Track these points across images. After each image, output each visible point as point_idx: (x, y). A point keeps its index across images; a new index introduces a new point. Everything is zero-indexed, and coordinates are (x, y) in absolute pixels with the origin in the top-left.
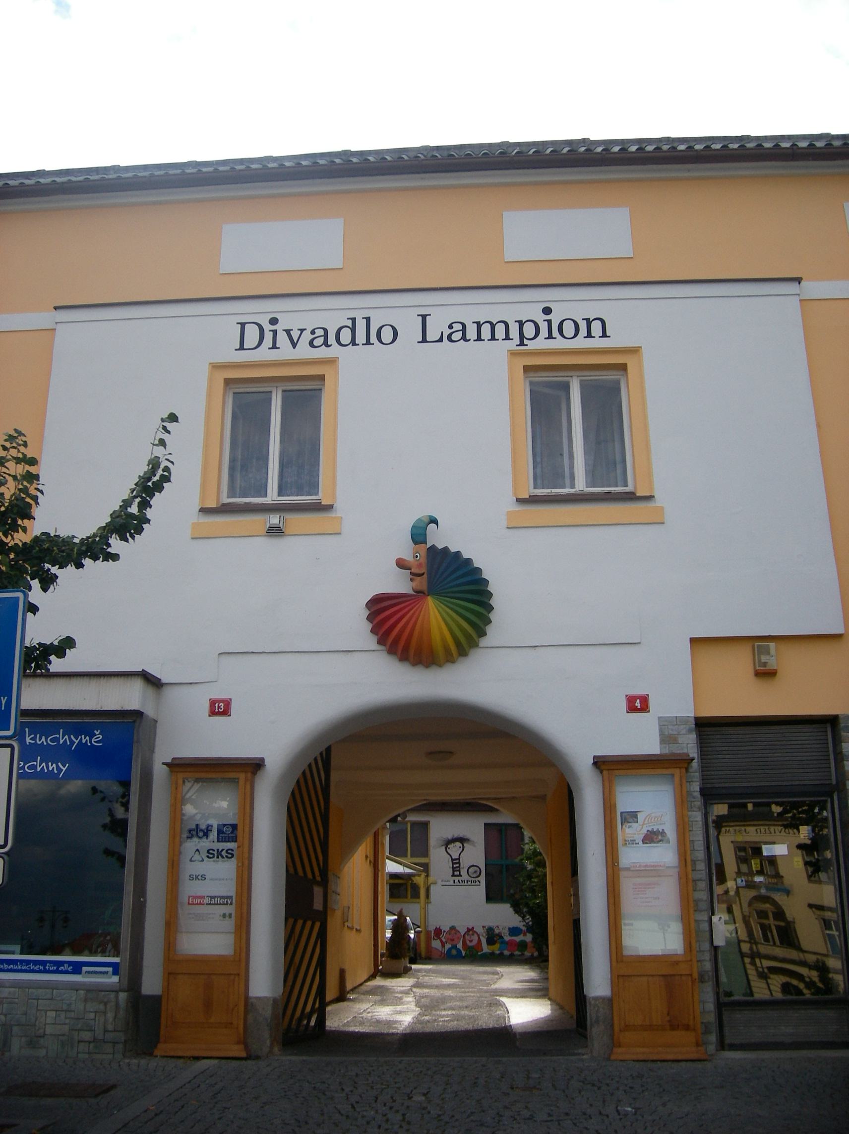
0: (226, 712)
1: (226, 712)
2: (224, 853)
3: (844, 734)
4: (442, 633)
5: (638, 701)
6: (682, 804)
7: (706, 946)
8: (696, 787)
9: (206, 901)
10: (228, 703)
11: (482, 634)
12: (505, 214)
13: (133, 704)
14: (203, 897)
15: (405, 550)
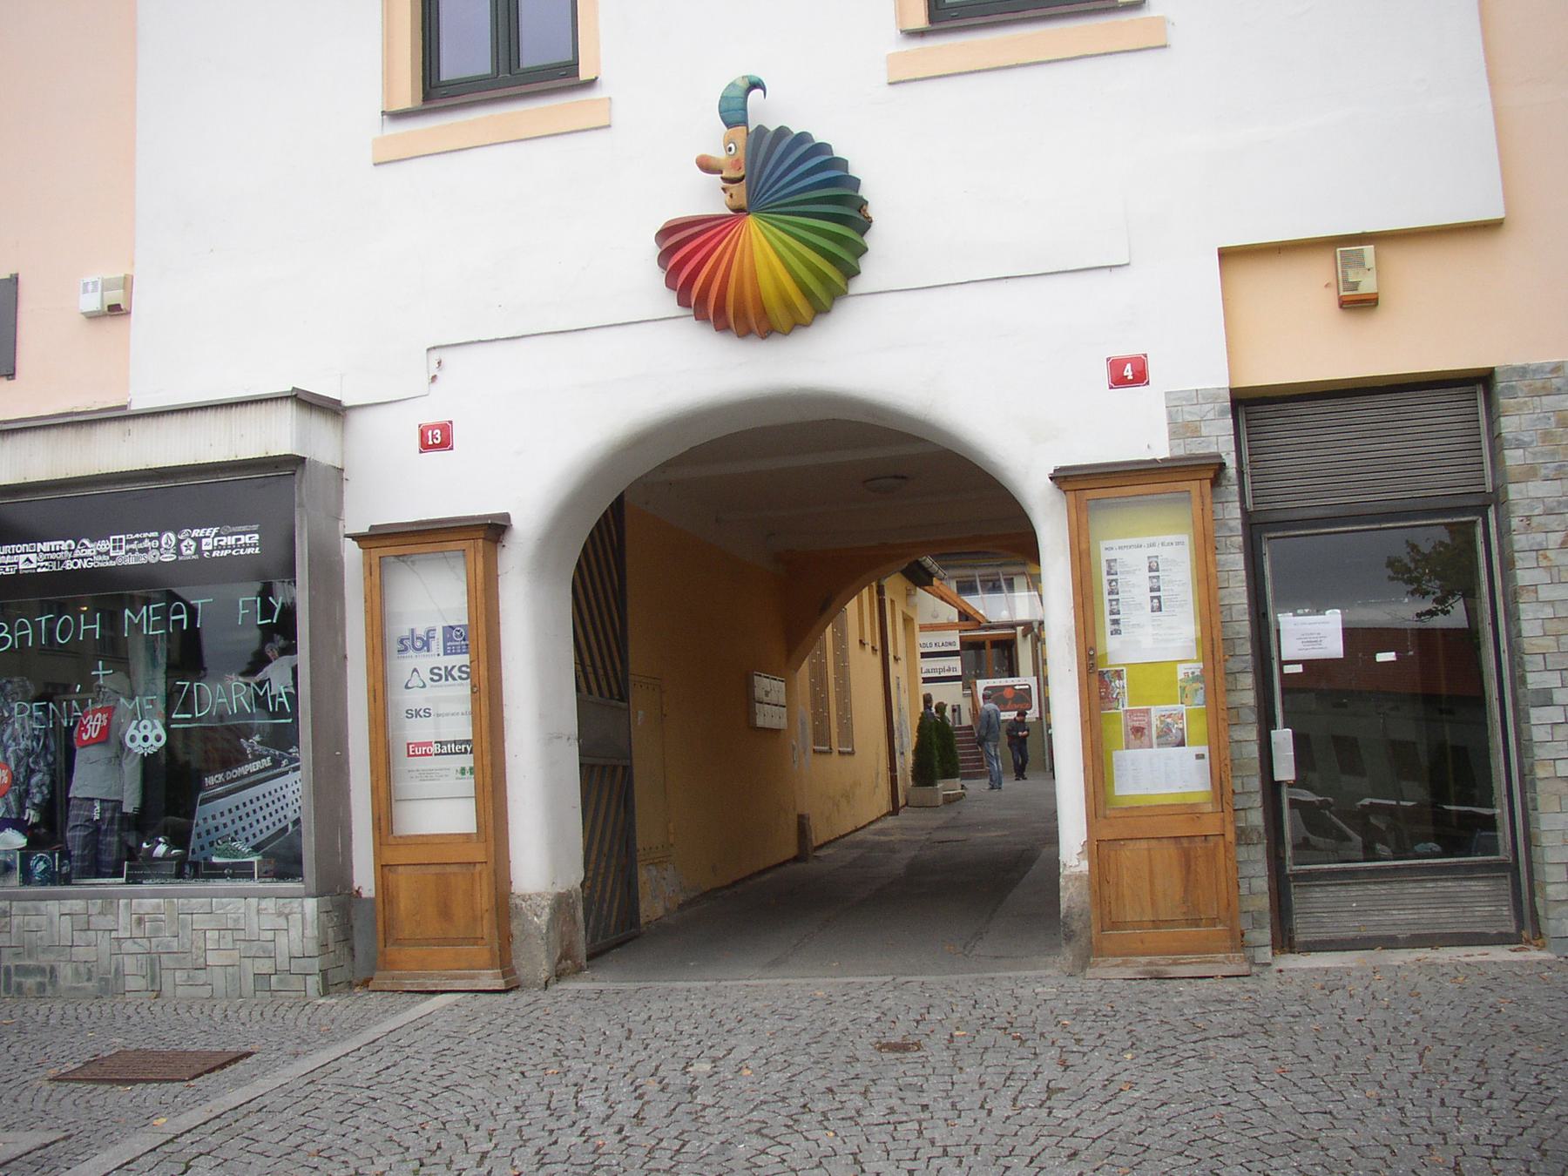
0: (446, 444)
1: (446, 444)
2: (455, 673)
3: (1503, 401)
4: (776, 280)
5: (1129, 366)
6: (1206, 548)
7: (1255, 783)
8: (1233, 513)
9: (435, 749)
10: (446, 429)
11: (851, 273)
12: (1117, 793)
13: (282, 445)
14: (430, 744)
15: (714, 139)
